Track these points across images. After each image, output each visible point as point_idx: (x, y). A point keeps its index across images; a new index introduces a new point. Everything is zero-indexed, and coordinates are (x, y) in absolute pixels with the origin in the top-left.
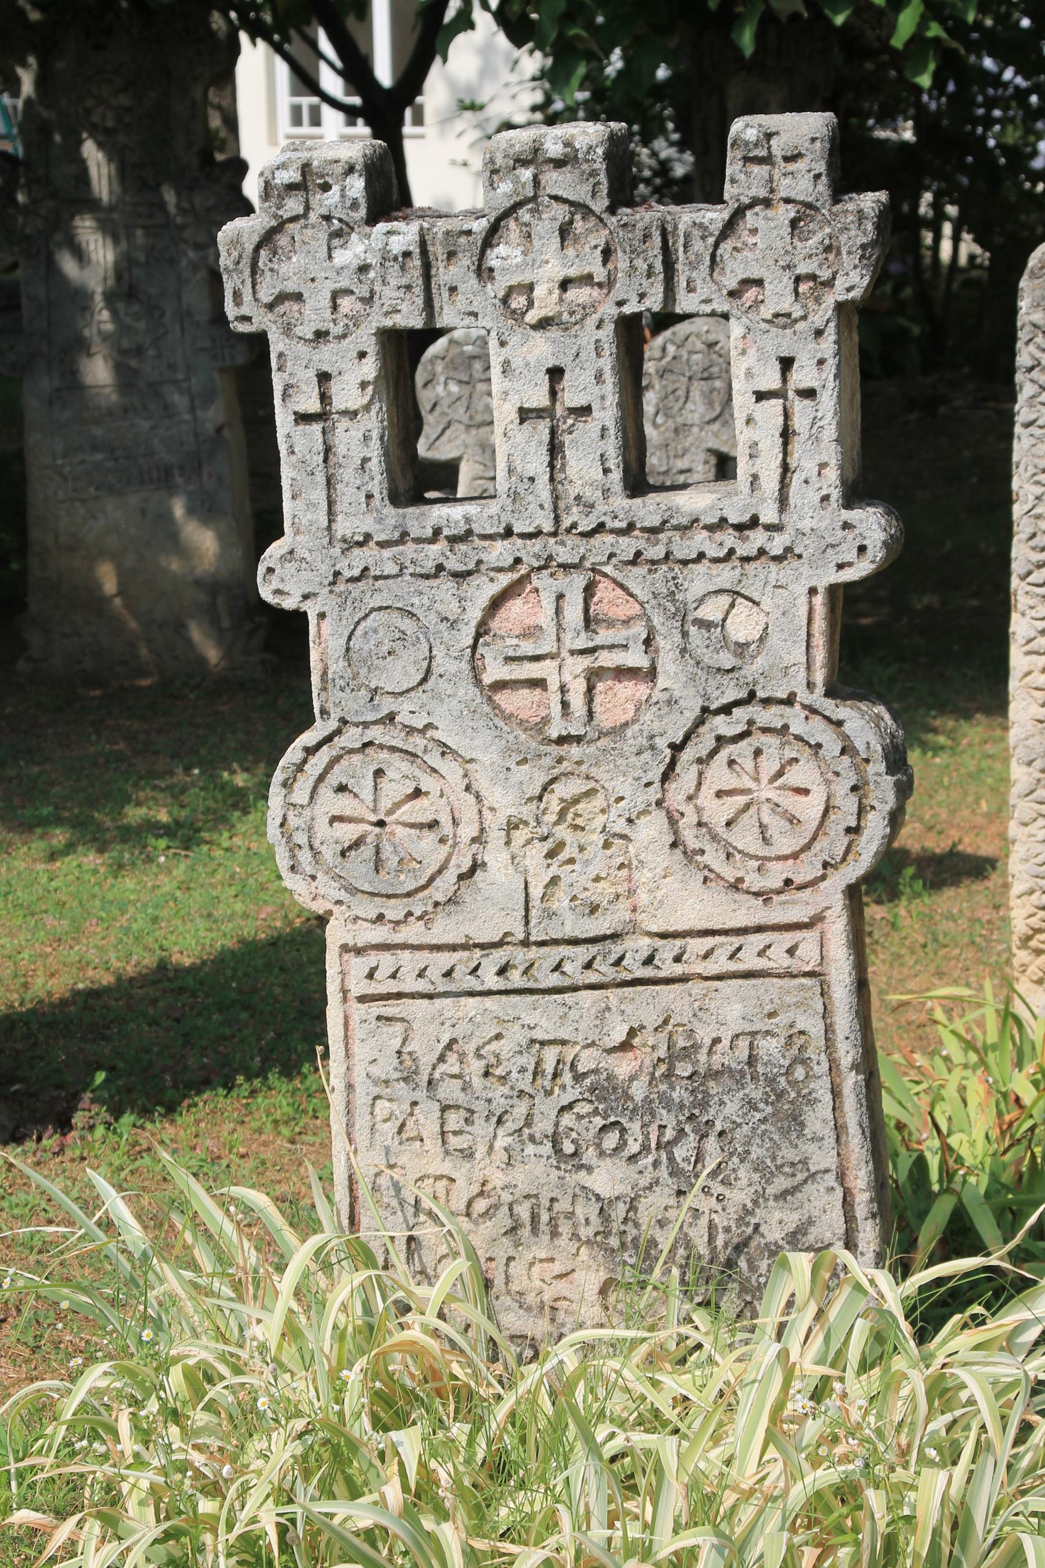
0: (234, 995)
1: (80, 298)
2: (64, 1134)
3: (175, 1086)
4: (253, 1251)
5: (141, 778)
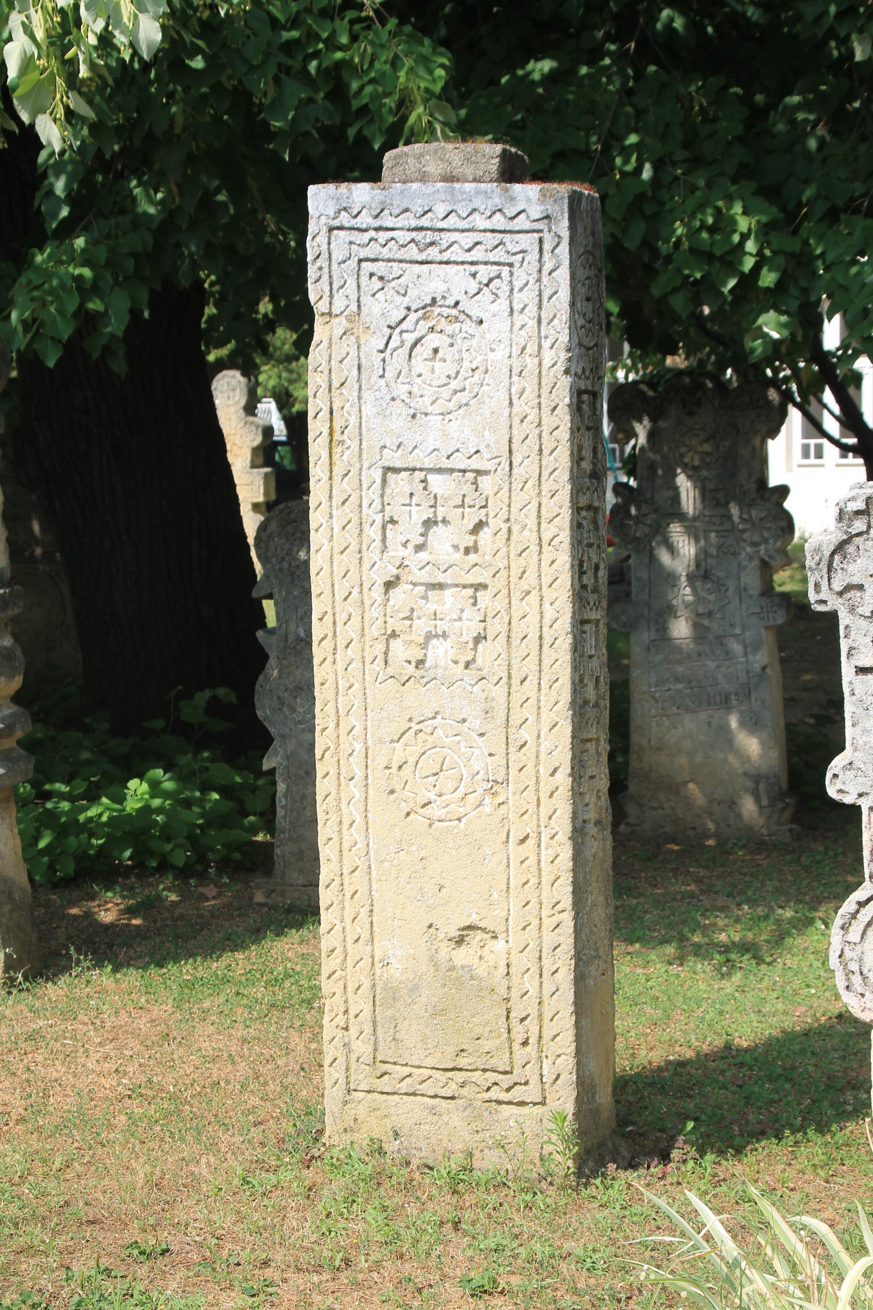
0: (779, 1071)
1: (671, 578)
2: (665, 1165)
3: (741, 1135)
4: (817, 1265)
5: (707, 910)
